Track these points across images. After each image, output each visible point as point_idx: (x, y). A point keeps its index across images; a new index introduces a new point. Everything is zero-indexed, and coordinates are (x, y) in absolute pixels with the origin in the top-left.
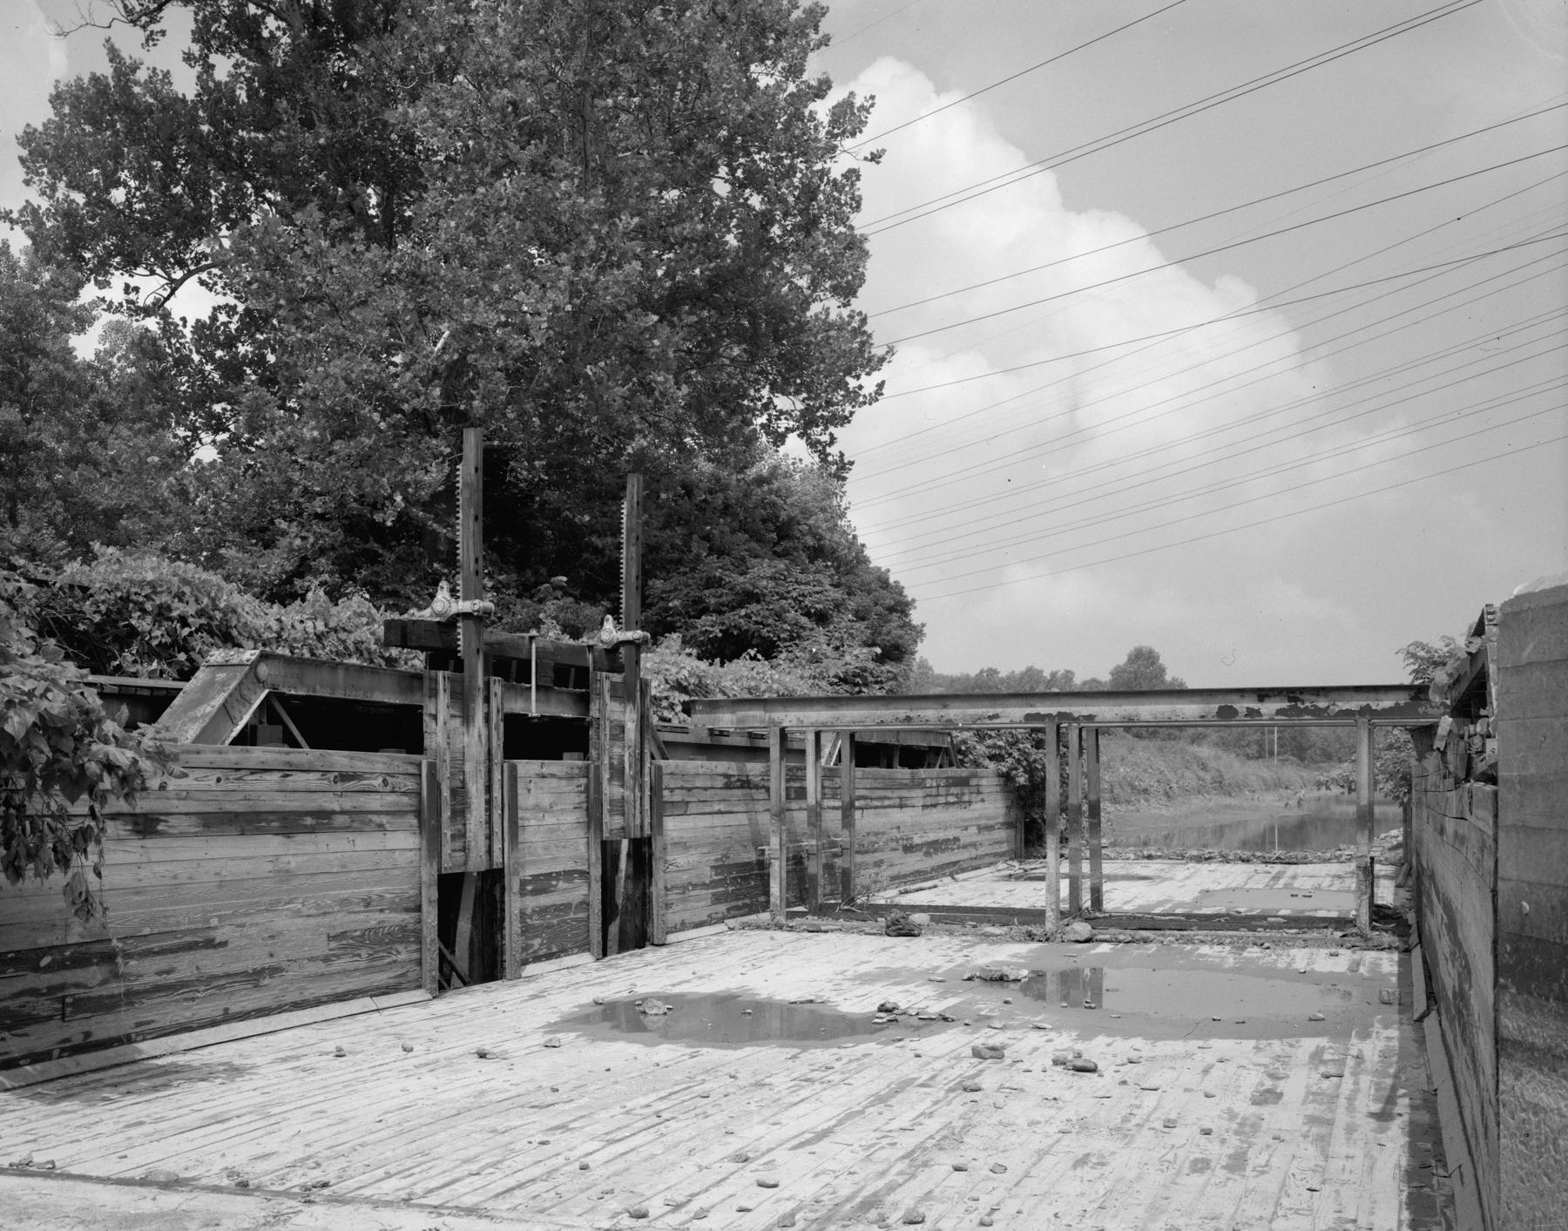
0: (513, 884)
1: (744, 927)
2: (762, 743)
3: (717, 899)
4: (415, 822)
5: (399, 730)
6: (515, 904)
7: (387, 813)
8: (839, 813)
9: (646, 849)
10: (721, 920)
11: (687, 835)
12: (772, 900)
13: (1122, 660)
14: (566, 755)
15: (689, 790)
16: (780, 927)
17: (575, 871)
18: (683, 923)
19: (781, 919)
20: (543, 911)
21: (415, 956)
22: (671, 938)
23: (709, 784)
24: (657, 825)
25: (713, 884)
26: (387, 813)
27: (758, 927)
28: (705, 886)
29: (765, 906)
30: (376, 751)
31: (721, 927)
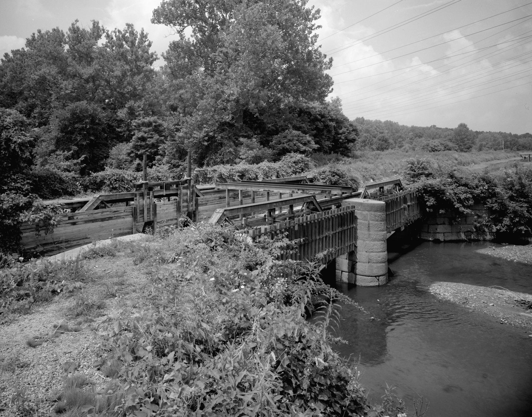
24: (197, 208)
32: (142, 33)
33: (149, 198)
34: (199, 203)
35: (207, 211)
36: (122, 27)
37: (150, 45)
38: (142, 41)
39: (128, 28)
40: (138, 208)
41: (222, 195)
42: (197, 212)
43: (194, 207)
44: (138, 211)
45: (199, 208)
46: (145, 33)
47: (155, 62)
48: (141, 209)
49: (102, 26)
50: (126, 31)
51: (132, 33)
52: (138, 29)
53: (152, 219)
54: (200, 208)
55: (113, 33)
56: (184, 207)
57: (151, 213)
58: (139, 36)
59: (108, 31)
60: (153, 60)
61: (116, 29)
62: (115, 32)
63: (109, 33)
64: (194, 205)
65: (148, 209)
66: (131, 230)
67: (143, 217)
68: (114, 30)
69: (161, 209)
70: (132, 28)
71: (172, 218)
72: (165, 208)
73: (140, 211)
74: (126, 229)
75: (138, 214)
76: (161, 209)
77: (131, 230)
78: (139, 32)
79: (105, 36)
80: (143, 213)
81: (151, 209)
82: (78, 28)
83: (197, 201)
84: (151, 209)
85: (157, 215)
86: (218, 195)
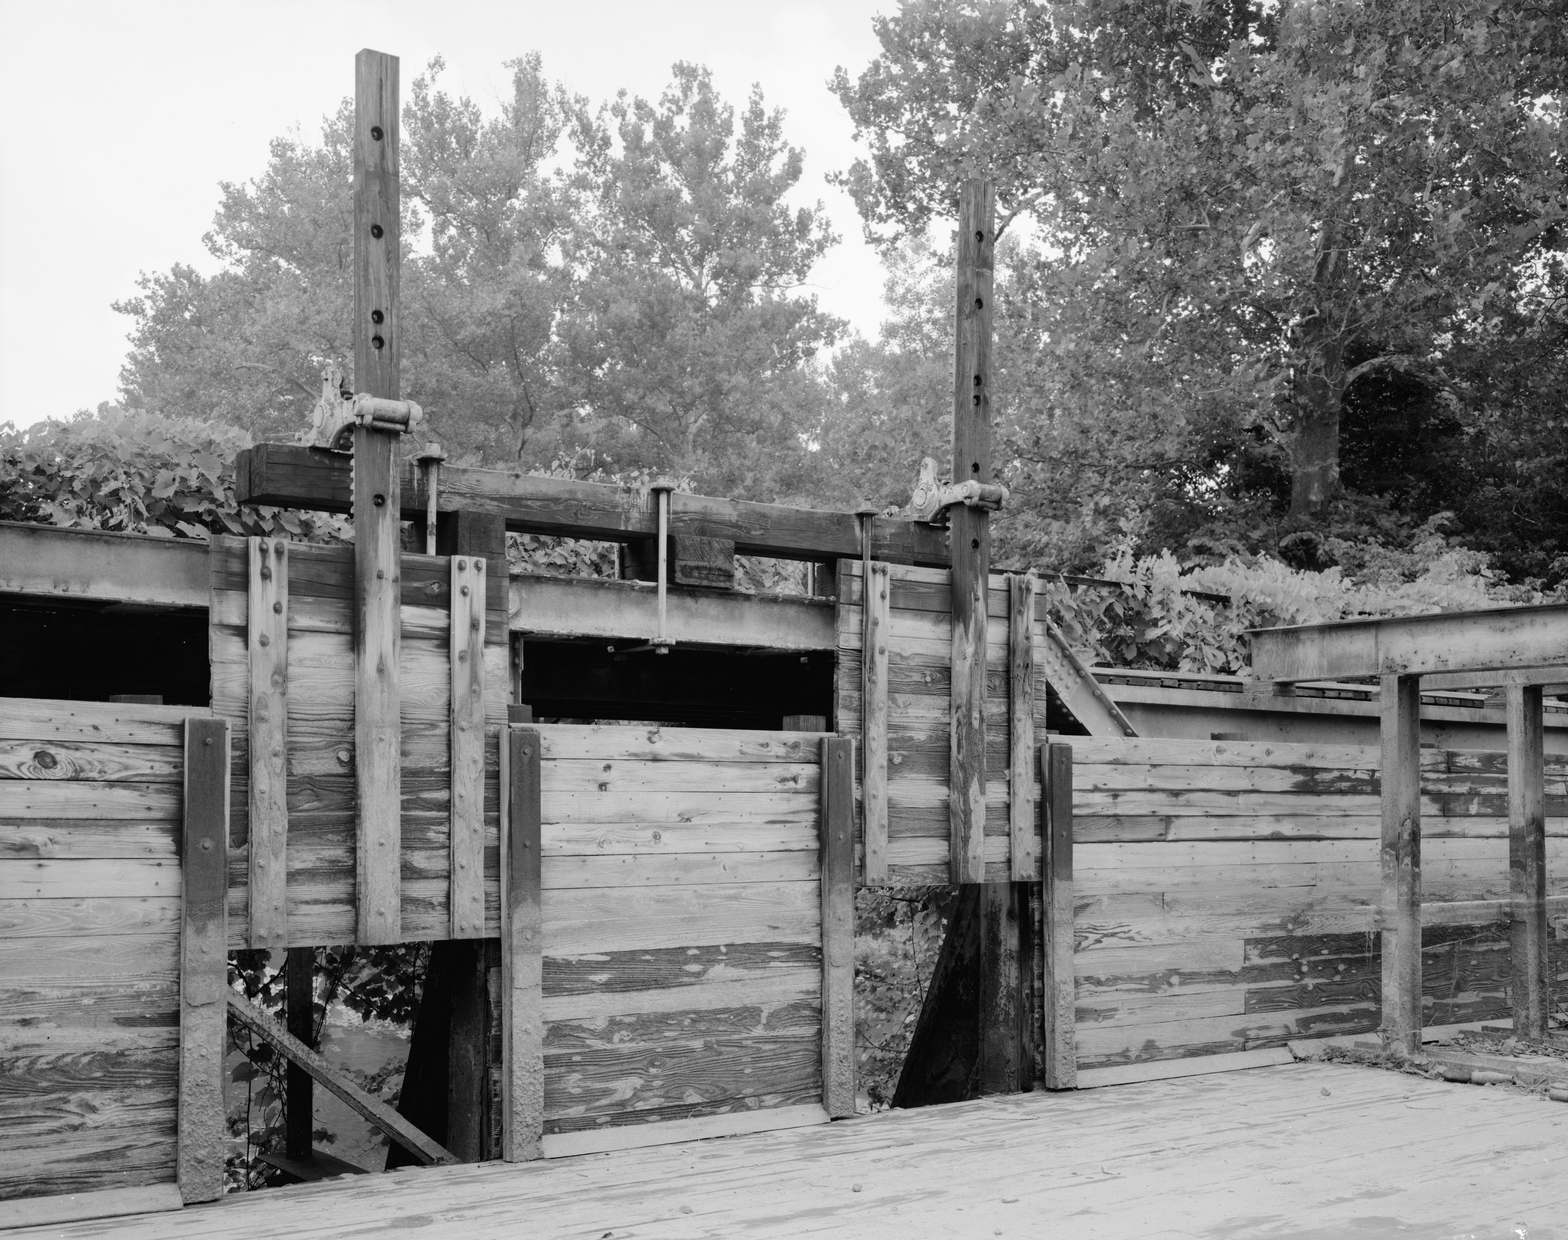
0: (524, 970)
1: (1331, 1056)
2: (1492, 716)
3: (1266, 1001)
4: (163, 842)
5: (155, 655)
6: (528, 1012)
7: (50, 822)
8: (1507, 842)
9: (1035, 904)
10: (1283, 1041)
11: (1163, 881)
12: (1386, 1010)
13: (846, 111)
14: (787, 720)
15: (1176, 793)
16: (1398, 1065)
17: (772, 946)
18: (1150, 1046)
19: (1402, 1049)
20: (645, 1025)
21: (164, 1114)
22: (1084, 1078)
23: (1245, 784)
24: (1053, 859)
25: (1250, 973)
26: (50, 822)
27: (1358, 1061)
28: (1223, 976)
29: (1373, 1021)
30: (105, 699)
31: (1280, 1055)
32: (758, 114)
33: (443, 640)
34: (1083, 800)
35: (1163, 902)
36: (655, 87)
37: (793, 171)
38: (754, 154)
39: (686, 90)
40: (268, 740)
41: (1337, 754)
42: (1060, 895)
43: (1027, 844)
44: (268, 781)
45: (1083, 856)
46: (769, 113)
47: (818, 263)
48: (323, 764)
49: (560, 89)
50: (674, 101)
51: (704, 112)
52: (732, 97)
53: (471, 921)
54: (1093, 863)
55: (608, 115)
56: (900, 819)
57: (471, 834)
58: (739, 131)
59: (583, 101)
60: (808, 254)
61: (622, 94)
62: (619, 111)
63: (592, 113)
64: (1024, 817)
65: (411, 779)
66: (144, 1040)
67: (350, 871)
68: (613, 99)
69: (607, 805)
70: (704, 87)
71: (753, 934)
72: (665, 806)
73: (296, 785)
74: (65, 1012)
75: (270, 819)
76: (607, 805)
77: (144, 1040)
78: (742, 108)
79: (573, 133)
80: (349, 826)
81: (469, 788)
82: (441, 101)
83: (1053, 777)
84: (469, 788)
85: (553, 876)
86: (1293, 750)
